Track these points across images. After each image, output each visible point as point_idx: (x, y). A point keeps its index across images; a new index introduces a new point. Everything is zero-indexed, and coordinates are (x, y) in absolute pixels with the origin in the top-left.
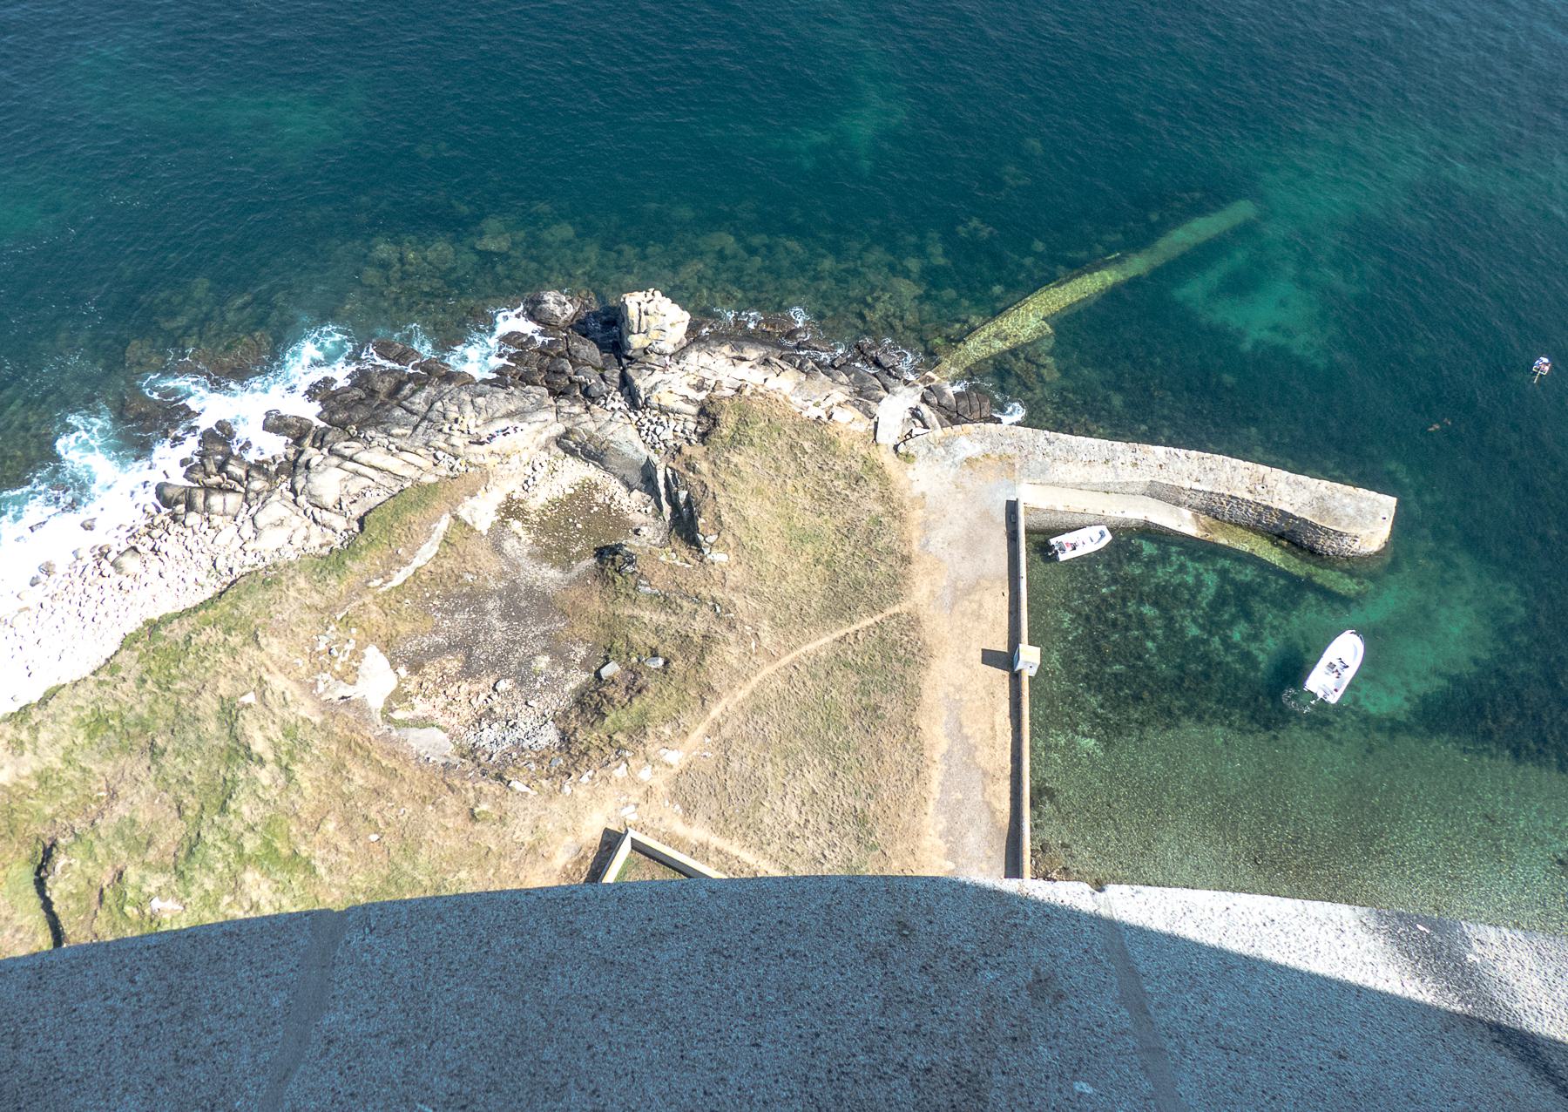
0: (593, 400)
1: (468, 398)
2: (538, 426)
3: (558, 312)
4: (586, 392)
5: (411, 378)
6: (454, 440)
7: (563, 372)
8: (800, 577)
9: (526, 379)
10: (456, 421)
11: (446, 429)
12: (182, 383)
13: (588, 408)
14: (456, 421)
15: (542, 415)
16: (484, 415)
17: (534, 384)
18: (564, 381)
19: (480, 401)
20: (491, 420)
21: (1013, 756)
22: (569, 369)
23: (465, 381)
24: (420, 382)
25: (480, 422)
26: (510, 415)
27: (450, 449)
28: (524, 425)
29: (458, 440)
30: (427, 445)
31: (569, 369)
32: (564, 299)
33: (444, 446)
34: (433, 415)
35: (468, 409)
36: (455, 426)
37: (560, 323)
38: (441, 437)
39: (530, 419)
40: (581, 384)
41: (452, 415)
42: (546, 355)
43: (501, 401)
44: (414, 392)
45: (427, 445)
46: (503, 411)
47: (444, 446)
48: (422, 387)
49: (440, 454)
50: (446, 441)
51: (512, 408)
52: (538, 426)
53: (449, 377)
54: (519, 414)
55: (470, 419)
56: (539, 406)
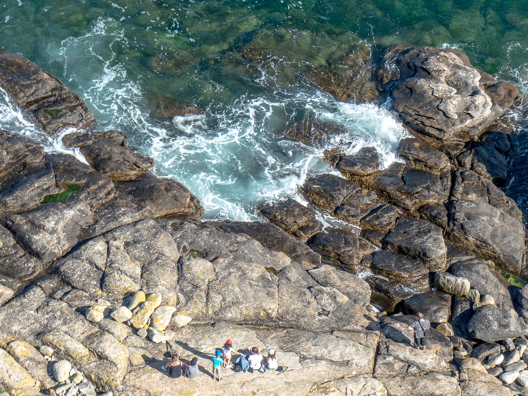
0: (478, 346)
1: (172, 253)
2: (321, 369)
3: (453, 106)
4: (465, 321)
5: (52, 164)
6: (111, 347)
7: (421, 257)
8: (167, 313)
9: (326, 248)
10: (128, 299)
11: (97, 313)
12: (252, 221)
13: (457, 364)
14: (128, 299)
15: (340, 349)
16: (198, 307)
17: (344, 265)
18: (413, 283)
19: (200, 267)
20: (212, 323)
21: (76, 250)
22: (438, 250)
23: (183, 215)
24: (70, 182)
25: (183, 320)
26: (260, 323)
27: (92, 364)
28: (290, 360)
29: (118, 350)
30: (40, 336)
31: (438, 250)
32: (475, 78)
33: (80, 350)
34: (77, 269)
35: (166, 278)
36: (125, 313)
37: (450, 136)
38: (80, 327)
39: (309, 348)
40: (456, 299)
41: (123, 283)
42: (394, 202)
43: (253, 282)
44: (49, 203)
45: (40, 336)
46: (247, 309)
47: (80, 350)
48: (71, 195)
49: (64, 369)
50: (88, 340)
51: (273, 307)
52: (321, 369)
53: (142, 189)
54: (287, 329)
55: (165, 314)
56: (338, 325)
